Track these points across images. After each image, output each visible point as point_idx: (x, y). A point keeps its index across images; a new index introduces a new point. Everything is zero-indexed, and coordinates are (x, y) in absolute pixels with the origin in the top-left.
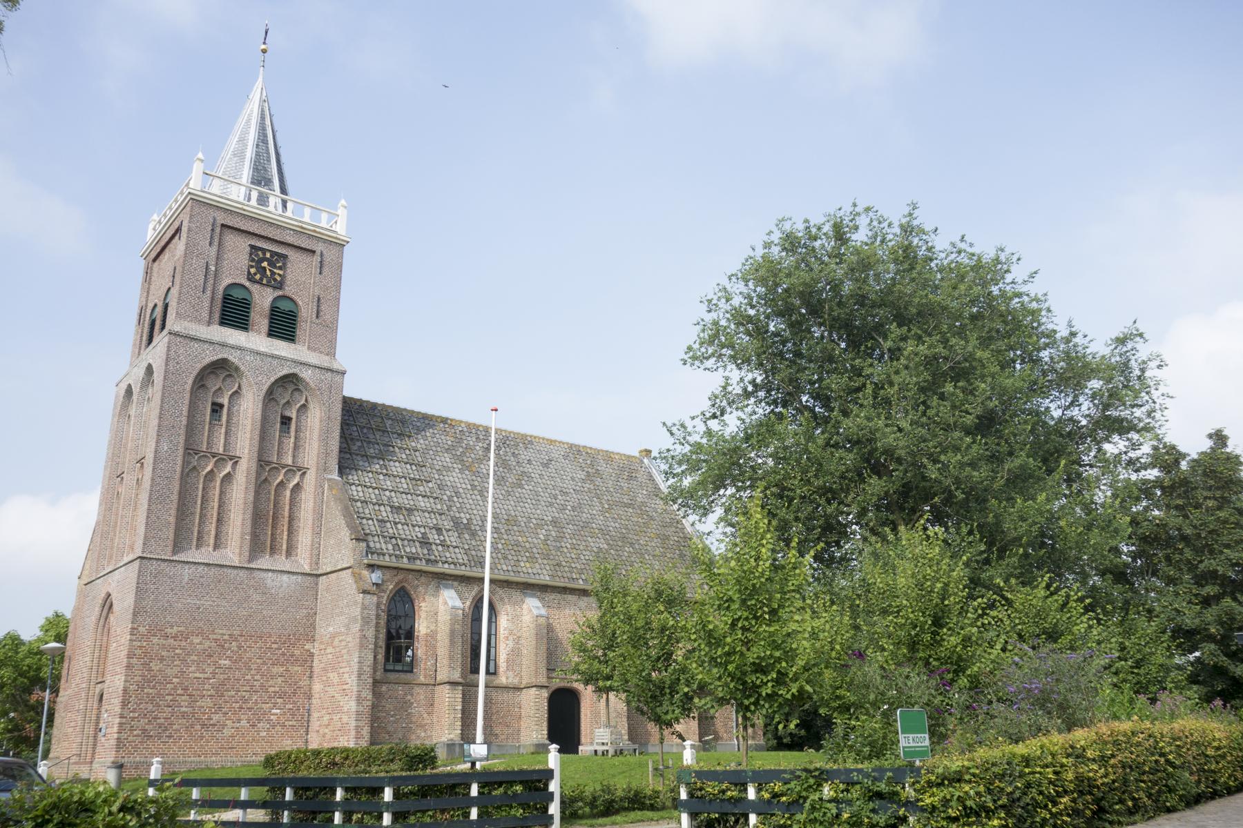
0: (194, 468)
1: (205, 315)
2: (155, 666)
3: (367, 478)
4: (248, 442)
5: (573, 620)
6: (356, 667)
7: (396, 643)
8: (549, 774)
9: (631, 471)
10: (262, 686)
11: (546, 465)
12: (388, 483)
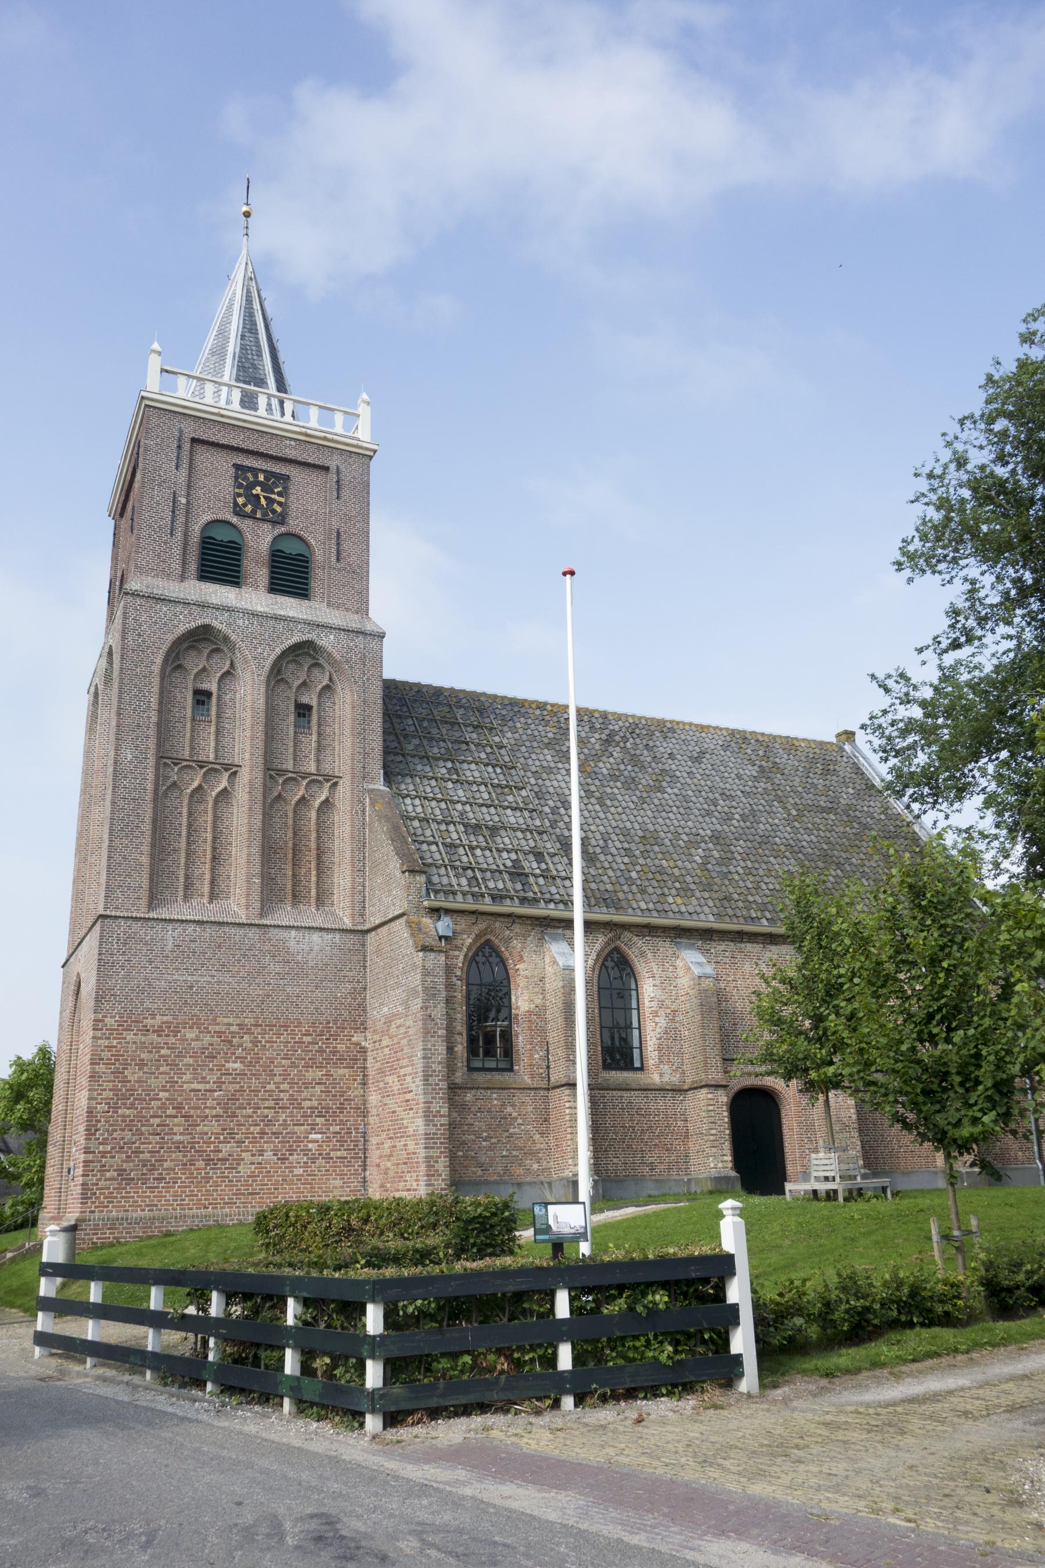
0: (174, 784)
1: (176, 567)
2: (132, 1075)
3: (429, 788)
4: (248, 743)
5: (754, 976)
6: (420, 1065)
7: (483, 1031)
8: (725, 1264)
9: (826, 763)
10: (292, 1099)
11: (697, 760)
12: (461, 793)
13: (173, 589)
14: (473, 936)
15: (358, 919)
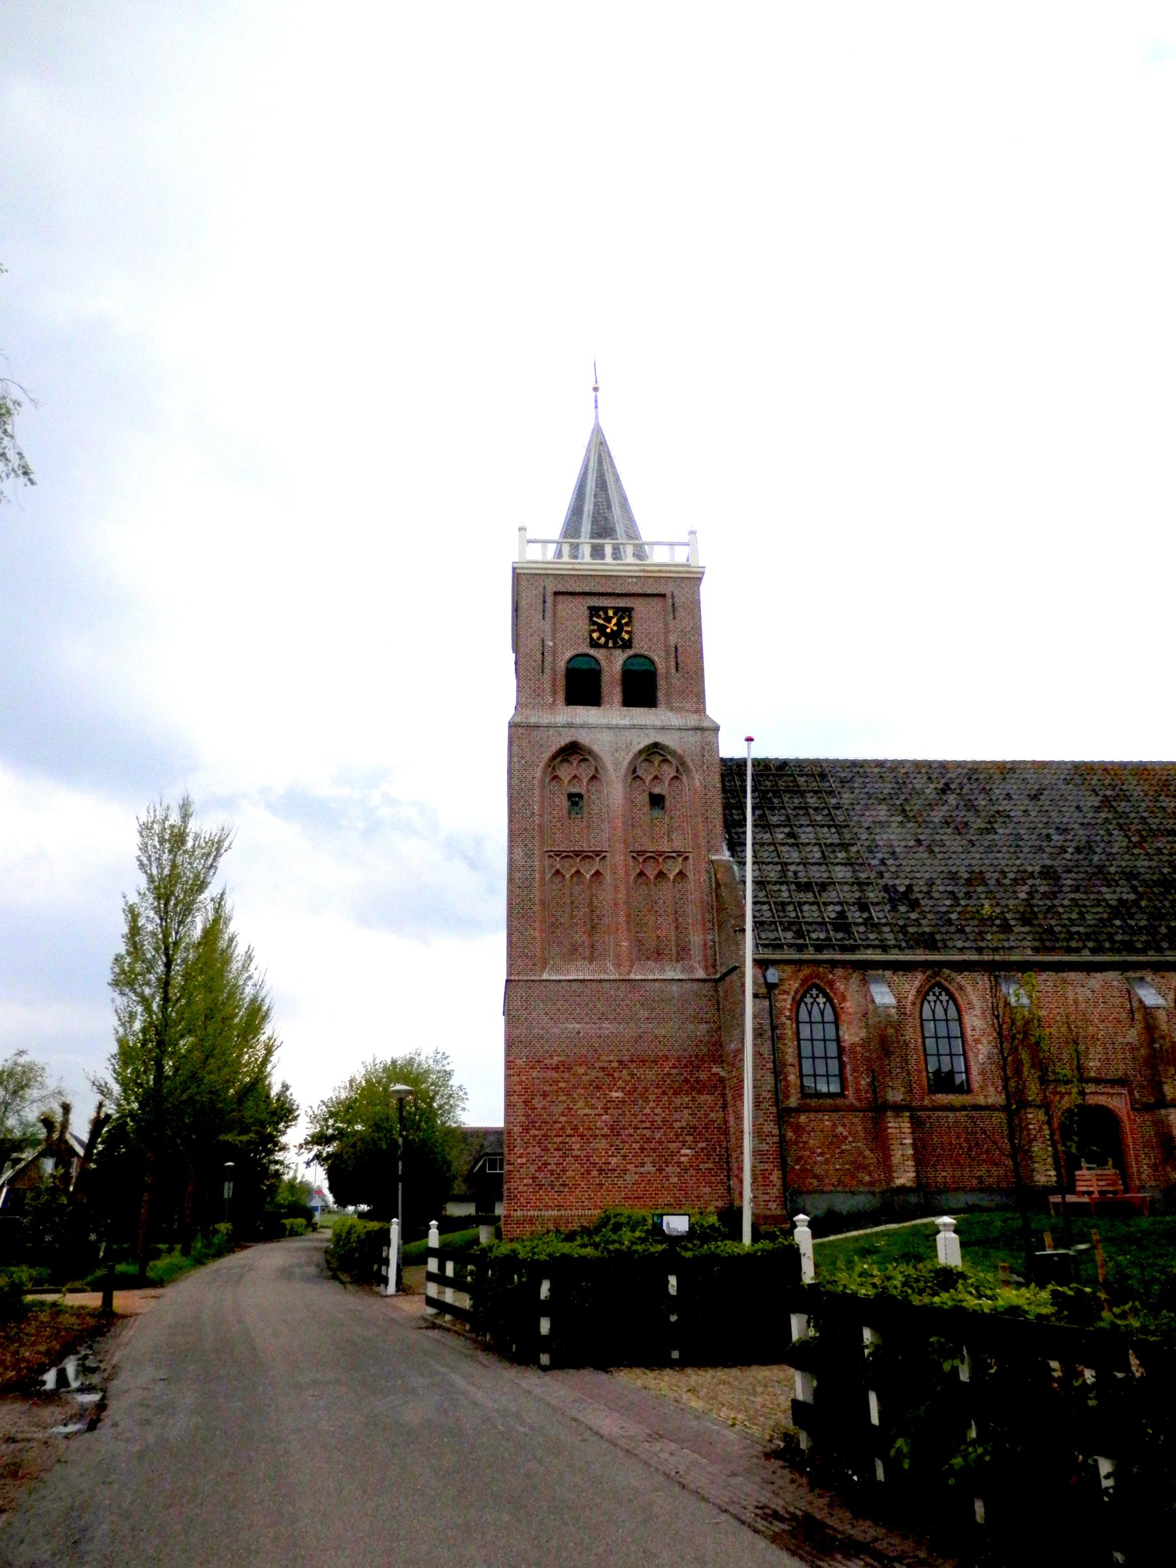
2: (538, 1102)
10: (664, 1121)
11: (1035, 797)
13: (546, 719)
14: (799, 981)
15: (711, 970)
